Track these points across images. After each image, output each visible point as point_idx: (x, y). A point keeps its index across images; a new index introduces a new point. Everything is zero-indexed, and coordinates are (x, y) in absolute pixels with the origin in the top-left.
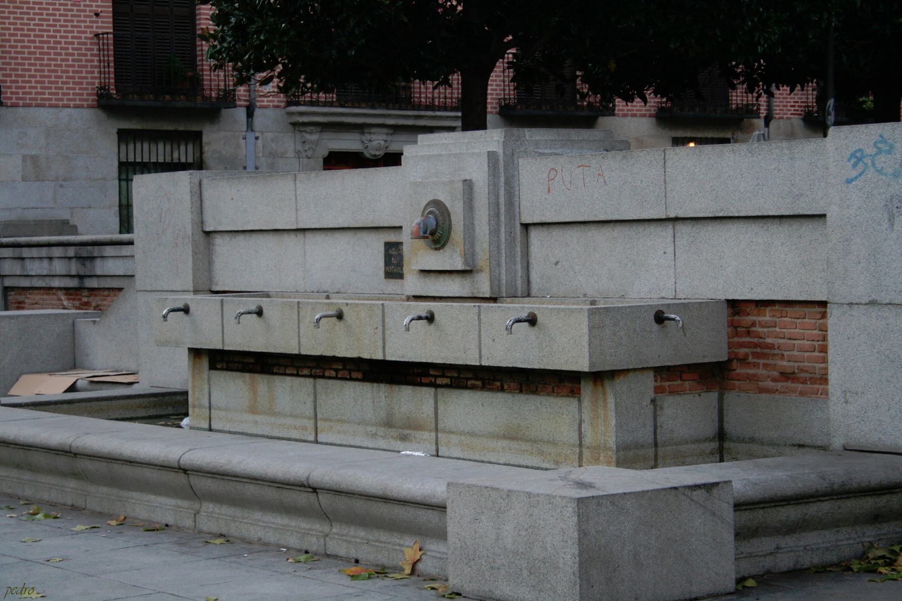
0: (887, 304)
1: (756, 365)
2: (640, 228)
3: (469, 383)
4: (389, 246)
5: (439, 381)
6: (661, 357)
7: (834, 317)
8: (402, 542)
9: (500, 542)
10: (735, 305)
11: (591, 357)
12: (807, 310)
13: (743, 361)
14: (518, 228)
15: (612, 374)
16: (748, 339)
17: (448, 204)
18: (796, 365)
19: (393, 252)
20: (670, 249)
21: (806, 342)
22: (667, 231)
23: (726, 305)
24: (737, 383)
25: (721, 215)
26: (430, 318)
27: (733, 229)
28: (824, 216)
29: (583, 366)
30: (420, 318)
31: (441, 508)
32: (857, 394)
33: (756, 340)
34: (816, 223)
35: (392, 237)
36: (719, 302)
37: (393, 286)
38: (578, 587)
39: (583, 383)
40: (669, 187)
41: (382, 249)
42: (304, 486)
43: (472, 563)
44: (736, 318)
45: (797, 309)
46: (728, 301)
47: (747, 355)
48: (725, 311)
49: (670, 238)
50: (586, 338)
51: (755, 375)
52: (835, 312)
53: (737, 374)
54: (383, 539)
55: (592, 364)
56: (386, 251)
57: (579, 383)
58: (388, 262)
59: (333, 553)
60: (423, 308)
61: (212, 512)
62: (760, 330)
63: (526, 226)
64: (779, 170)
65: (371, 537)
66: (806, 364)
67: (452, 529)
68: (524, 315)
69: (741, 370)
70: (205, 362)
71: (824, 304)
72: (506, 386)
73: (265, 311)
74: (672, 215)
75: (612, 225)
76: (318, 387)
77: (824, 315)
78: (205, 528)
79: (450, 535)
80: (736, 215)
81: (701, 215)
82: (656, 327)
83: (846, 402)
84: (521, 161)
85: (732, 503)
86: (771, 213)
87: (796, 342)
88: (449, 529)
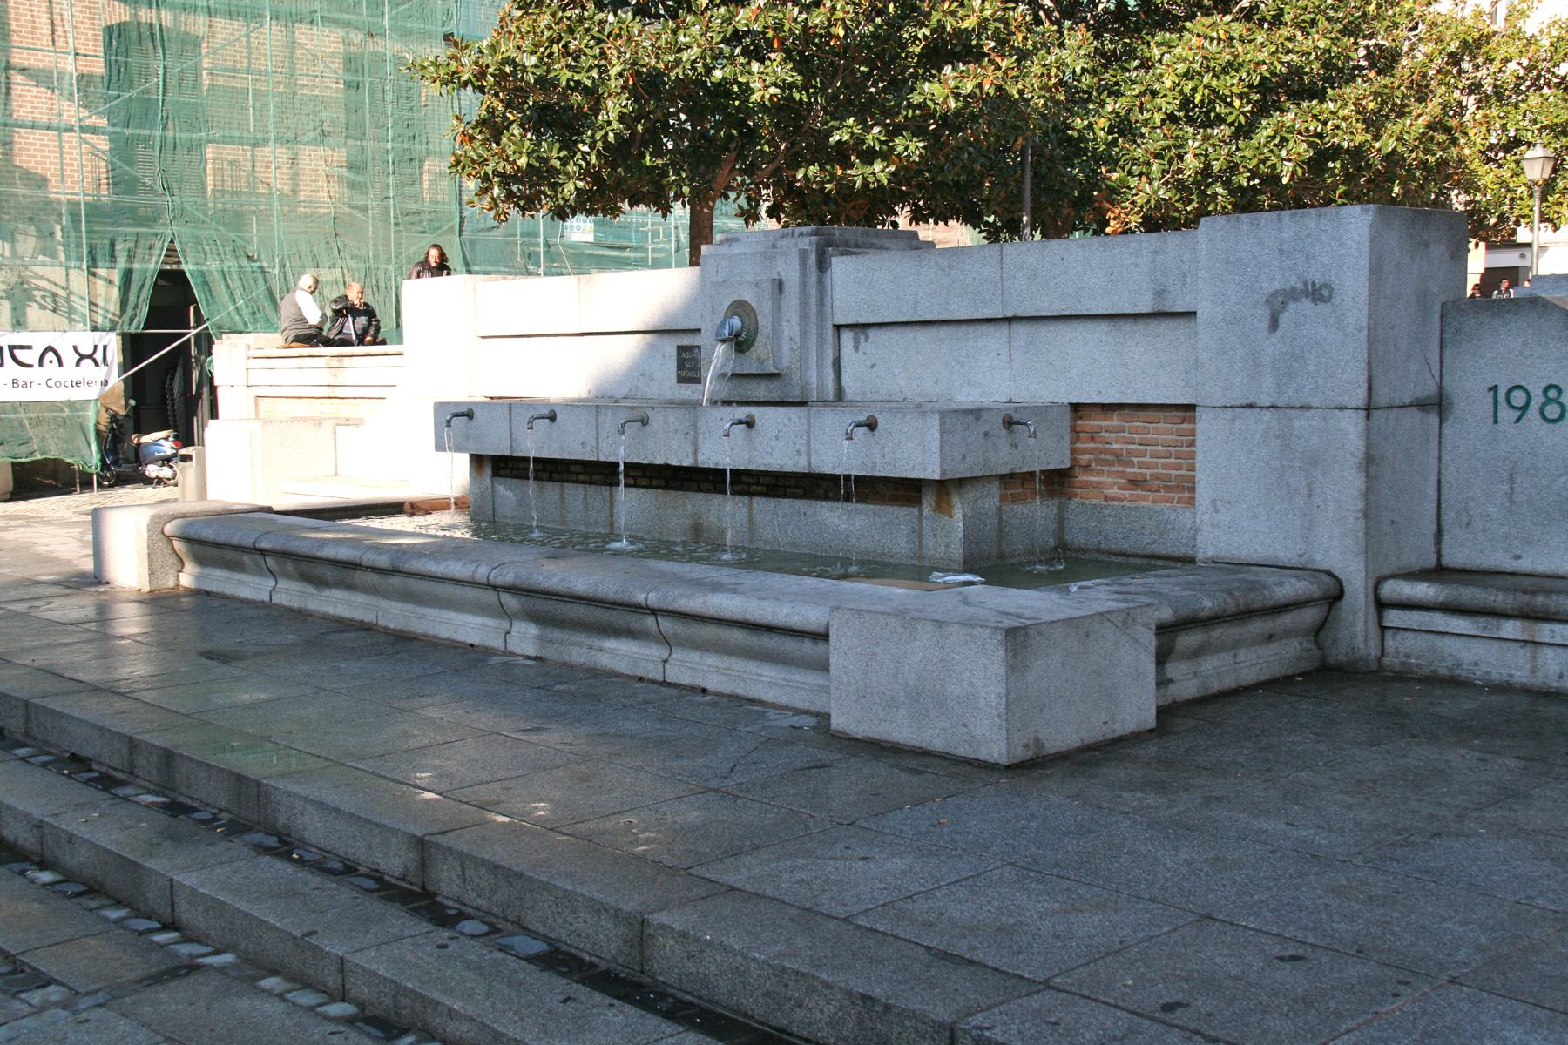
0: (1268, 407)
1: (1100, 473)
2: (971, 329)
3: (789, 490)
4: (681, 349)
5: (753, 488)
6: (968, 459)
7: (1205, 424)
8: (759, 671)
9: (900, 677)
10: (1076, 408)
11: (941, 465)
12: (1161, 414)
13: (1087, 468)
14: (830, 331)
15: (960, 483)
16: (1092, 445)
17: (754, 305)
18: (1149, 472)
19: (685, 355)
20: (1004, 352)
21: (1160, 448)
22: (1002, 332)
23: (1068, 409)
24: (1079, 491)
25: (1067, 313)
26: (750, 423)
27: (1079, 329)
28: (1194, 313)
29: (931, 470)
30: (740, 422)
31: (823, 636)
32: (1229, 503)
33: (1100, 446)
34: (1182, 326)
35: (686, 341)
36: (1062, 405)
37: (687, 392)
38: (1004, 732)
39: (924, 490)
40: (1007, 284)
41: (674, 352)
42: (642, 608)
43: (863, 700)
44: (1079, 422)
45: (1151, 414)
46: (1071, 404)
47: (1090, 461)
48: (1067, 415)
49: (1005, 339)
50: (937, 444)
51: (1100, 483)
52: (1204, 416)
53: (1081, 482)
54: (735, 667)
55: (943, 472)
56: (679, 354)
57: (920, 492)
58: (680, 366)
59: (675, 680)
60: (742, 412)
61: (525, 633)
62: (1107, 435)
63: (838, 328)
64: (1137, 265)
65: (720, 665)
66: (1160, 471)
67: (835, 661)
68: (863, 418)
69: (1083, 478)
70: (488, 471)
71: (1191, 408)
72: (831, 495)
73: (559, 416)
74: (1009, 314)
75: (936, 326)
76: (755, 505)
77: (1193, 420)
78: (517, 651)
79: (832, 668)
80: (1085, 313)
81: (1044, 314)
82: (1004, 432)
83: (1217, 512)
84: (834, 260)
85: (1154, 627)
86: (1126, 311)
87: (1148, 448)
88: (833, 661)
